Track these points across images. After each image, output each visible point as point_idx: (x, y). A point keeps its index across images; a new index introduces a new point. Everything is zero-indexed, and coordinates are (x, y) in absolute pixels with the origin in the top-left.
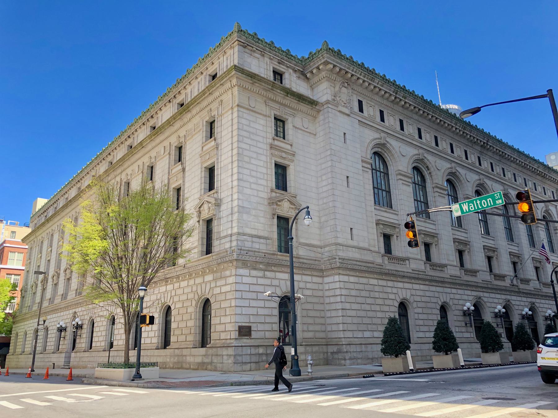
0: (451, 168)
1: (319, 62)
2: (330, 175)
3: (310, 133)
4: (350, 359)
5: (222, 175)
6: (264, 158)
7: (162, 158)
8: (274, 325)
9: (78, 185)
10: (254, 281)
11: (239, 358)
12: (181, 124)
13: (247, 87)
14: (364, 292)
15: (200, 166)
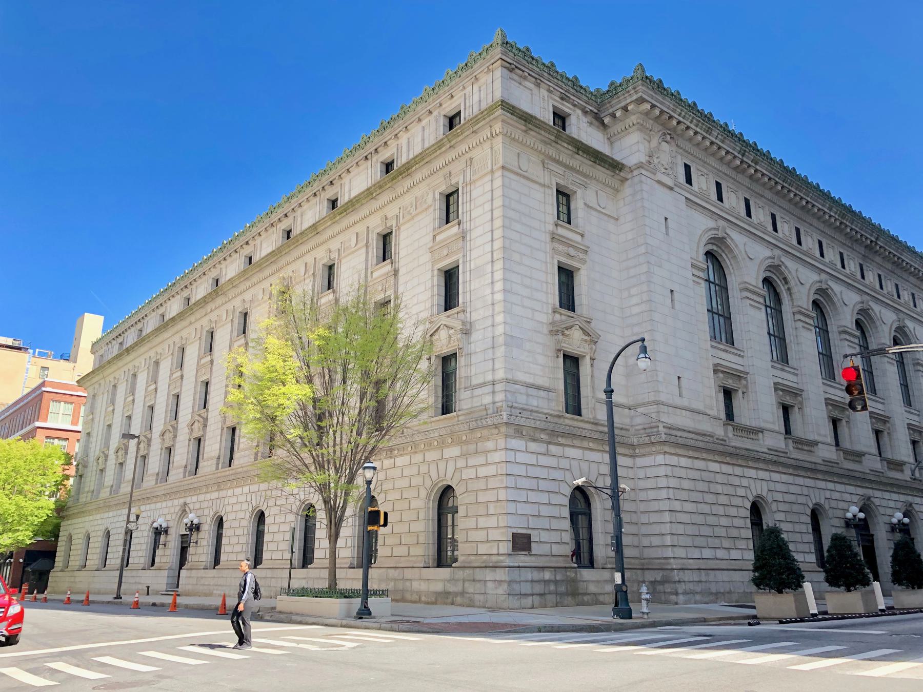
0: (821, 282)
1: (628, 99)
2: (644, 288)
3: (609, 216)
4: (685, 593)
7: (353, 252)
8: (563, 534)
9: (186, 293)
10: (532, 459)
11: (516, 587)
15: (429, 266)
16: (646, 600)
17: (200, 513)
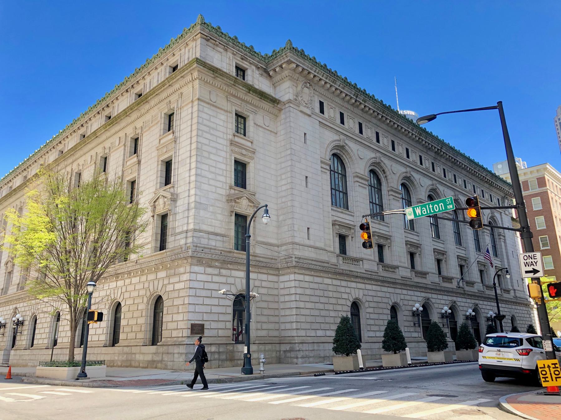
3: (271, 131)
4: (303, 357)
5: (179, 170)
6: (223, 154)
7: (117, 149)
8: (227, 323)
9: (25, 174)
10: (209, 278)
12: (139, 114)
13: (208, 81)
14: (318, 291)
16: (262, 362)
17: (24, 314)
